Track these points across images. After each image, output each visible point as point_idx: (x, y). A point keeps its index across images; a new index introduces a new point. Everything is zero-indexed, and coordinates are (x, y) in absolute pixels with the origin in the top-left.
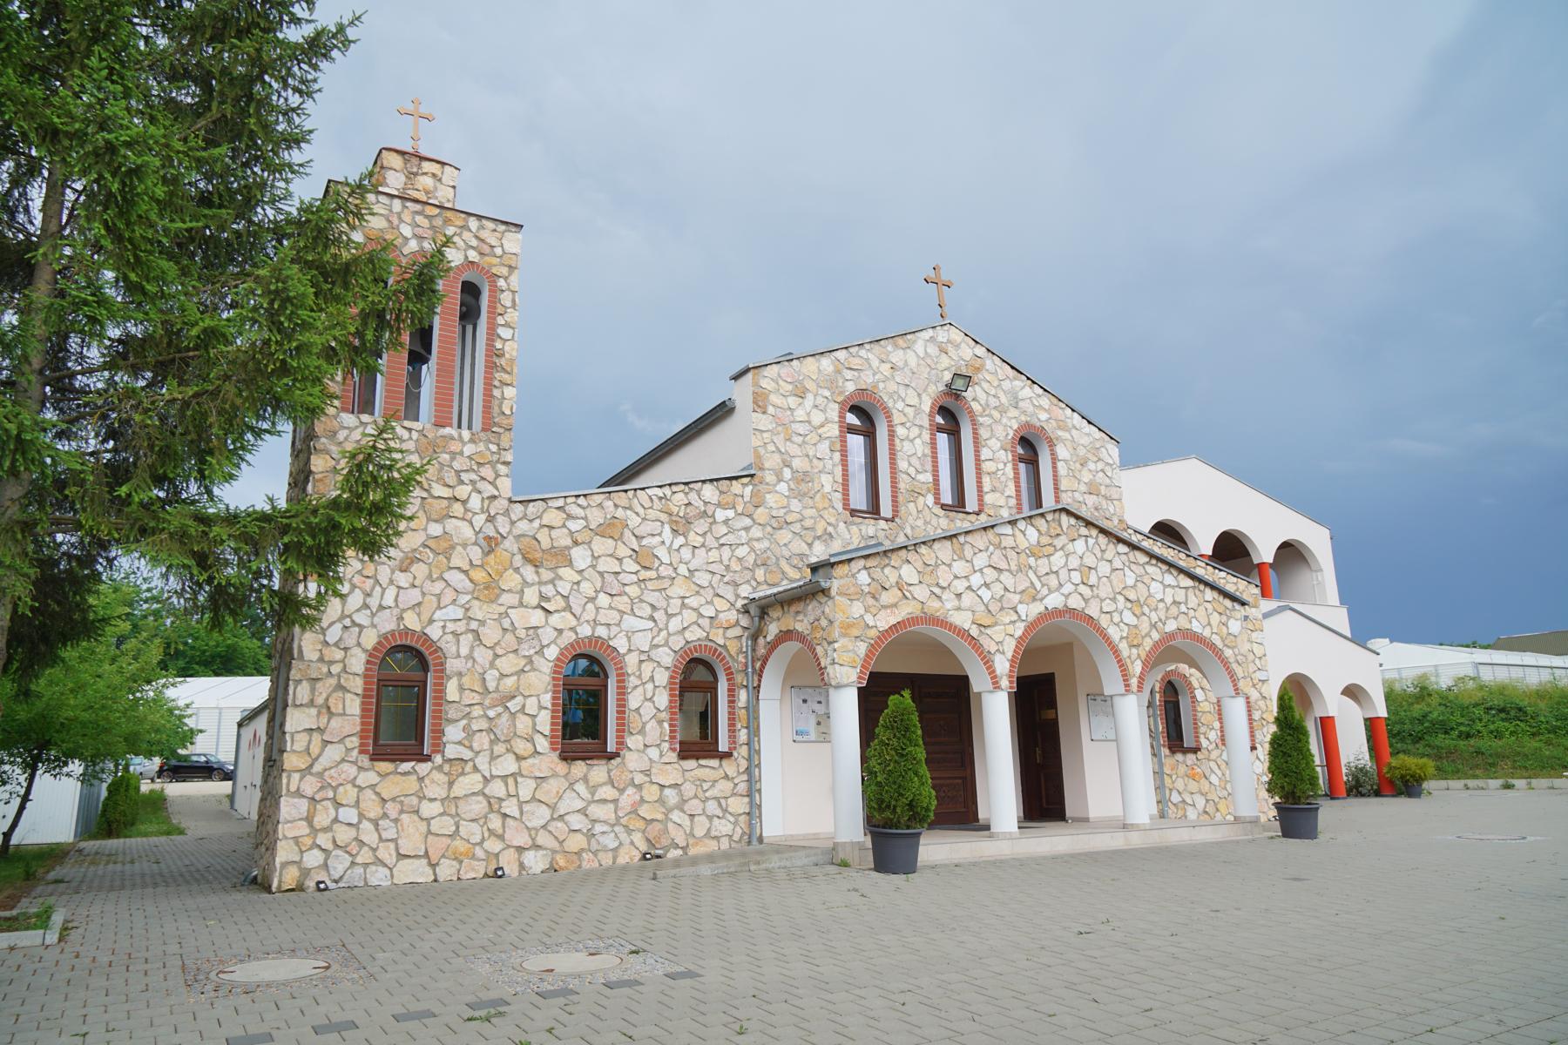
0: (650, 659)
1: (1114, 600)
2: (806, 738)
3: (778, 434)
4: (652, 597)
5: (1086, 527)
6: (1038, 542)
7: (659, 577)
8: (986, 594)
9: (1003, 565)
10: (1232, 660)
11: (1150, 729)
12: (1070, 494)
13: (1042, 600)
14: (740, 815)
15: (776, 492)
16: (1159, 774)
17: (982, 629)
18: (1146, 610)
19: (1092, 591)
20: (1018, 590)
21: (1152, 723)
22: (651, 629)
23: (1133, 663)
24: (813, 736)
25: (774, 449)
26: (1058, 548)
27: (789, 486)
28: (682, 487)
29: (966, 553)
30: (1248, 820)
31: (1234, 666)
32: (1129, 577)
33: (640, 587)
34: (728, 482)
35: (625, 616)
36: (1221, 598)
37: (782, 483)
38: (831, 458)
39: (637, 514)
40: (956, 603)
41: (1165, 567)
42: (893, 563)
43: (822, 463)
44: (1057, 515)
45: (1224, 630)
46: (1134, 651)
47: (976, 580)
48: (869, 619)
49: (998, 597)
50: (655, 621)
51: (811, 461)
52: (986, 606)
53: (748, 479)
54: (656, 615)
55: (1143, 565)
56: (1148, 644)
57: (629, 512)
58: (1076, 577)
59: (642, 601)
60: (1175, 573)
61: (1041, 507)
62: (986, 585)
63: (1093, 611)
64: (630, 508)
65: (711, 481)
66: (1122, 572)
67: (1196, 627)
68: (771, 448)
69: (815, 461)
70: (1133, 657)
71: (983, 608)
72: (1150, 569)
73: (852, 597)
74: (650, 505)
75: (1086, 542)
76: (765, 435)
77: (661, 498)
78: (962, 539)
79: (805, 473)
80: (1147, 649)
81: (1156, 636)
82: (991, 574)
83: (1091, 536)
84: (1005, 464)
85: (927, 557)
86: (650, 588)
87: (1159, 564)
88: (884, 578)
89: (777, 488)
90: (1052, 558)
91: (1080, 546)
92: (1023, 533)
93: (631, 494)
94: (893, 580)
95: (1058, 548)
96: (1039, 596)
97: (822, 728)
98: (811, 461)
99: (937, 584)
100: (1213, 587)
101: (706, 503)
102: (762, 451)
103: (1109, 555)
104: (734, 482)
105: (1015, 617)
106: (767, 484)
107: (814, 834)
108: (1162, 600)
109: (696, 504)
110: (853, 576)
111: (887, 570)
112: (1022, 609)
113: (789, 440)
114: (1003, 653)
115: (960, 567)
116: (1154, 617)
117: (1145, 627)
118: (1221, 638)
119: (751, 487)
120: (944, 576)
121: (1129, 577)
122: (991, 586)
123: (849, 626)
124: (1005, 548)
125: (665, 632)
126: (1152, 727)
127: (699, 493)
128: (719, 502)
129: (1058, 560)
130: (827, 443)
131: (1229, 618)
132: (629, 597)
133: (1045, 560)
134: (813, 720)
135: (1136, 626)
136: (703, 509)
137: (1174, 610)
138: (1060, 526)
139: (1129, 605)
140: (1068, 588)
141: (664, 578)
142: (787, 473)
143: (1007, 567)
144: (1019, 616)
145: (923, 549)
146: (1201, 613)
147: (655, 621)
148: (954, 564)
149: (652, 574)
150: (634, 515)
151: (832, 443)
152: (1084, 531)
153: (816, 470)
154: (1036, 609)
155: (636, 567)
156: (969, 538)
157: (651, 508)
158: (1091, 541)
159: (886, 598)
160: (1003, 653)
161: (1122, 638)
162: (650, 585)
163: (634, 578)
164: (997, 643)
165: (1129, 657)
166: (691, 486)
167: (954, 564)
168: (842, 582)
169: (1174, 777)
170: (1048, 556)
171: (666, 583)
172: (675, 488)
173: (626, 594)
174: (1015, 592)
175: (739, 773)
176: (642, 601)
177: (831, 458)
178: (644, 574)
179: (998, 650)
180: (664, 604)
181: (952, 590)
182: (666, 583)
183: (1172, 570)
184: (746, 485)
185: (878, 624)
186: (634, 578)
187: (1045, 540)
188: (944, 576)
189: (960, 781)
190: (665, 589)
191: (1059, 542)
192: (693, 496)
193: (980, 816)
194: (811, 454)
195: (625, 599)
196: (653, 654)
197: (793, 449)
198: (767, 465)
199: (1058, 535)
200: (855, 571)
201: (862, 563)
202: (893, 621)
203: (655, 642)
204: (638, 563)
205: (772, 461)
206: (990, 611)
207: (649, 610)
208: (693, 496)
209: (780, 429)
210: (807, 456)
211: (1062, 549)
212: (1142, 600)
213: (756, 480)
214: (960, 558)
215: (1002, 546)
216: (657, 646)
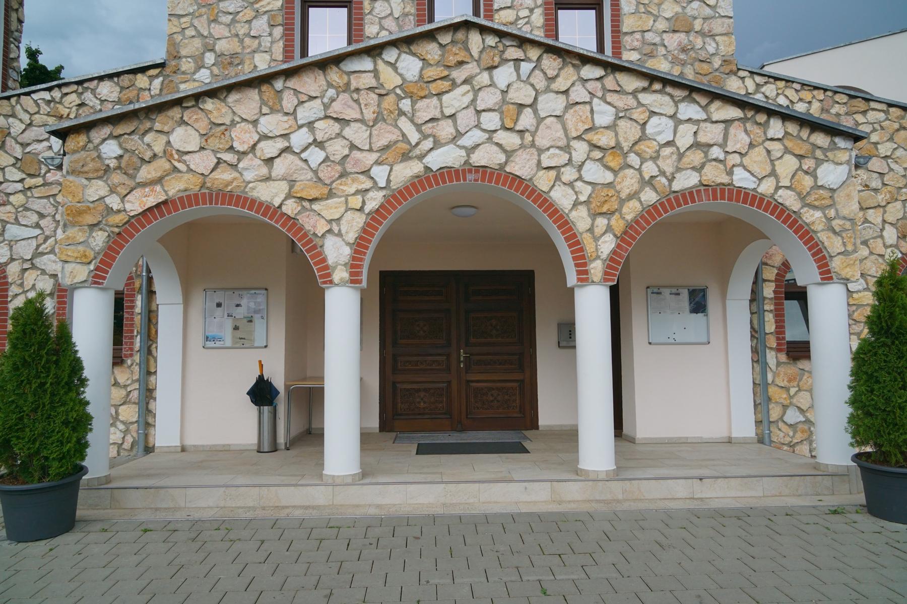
0: (34, 267)
1: (567, 149)
2: (218, 344)
3: (201, 16)
4: (37, 205)
5: (520, 46)
6: (421, 76)
7: (45, 184)
8: (315, 156)
9: (351, 113)
10: (818, 227)
11: (752, 327)
12: (638, 36)
13: (421, 157)
14: (132, 423)
15: (194, 80)
16: (761, 388)
17: (306, 204)
18: (633, 159)
19: (522, 138)
20: (375, 147)
21: (755, 322)
22: (36, 237)
23: (596, 239)
24: (228, 343)
25: (193, 33)
26: (459, 81)
27: (211, 72)
28: (75, 87)
29: (284, 103)
30: (831, 470)
31: (824, 237)
32: (602, 113)
33: (25, 195)
34: (131, 76)
35: (8, 226)
36: (805, 133)
37: (203, 70)
38: (270, 35)
39: (21, 120)
40: (264, 171)
41: (679, 93)
42: (158, 126)
43: (257, 41)
44: (460, 35)
45: (808, 181)
46: (601, 222)
47: (300, 138)
48: (114, 202)
49: (338, 158)
50: (42, 229)
51: (241, 41)
52: (315, 172)
53: (156, 71)
54: (43, 223)
55: (634, 93)
56: (631, 210)
57: (11, 120)
58: (491, 121)
59: (27, 209)
60: (703, 101)
61: (431, 19)
62: (320, 144)
63: (521, 167)
64: (13, 116)
65: (110, 76)
66: (588, 107)
67: (742, 179)
68: (190, 32)
69: (247, 41)
70: (598, 231)
71: (310, 175)
72: (646, 98)
73: (91, 175)
74: (36, 109)
75: (517, 69)
76: (183, 20)
77: (48, 102)
78: (279, 84)
79: (234, 55)
80: (629, 217)
81: (649, 196)
82: (325, 128)
83: (527, 59)
84: (531, 11)
85: (215, 113)
86: (36, 195)
87: (669, 89)
88: (142, 148)
89: (196, 76)
90: (445, 98)
91: (504, 75)
92: (393, 66)
93: (13, 100)
94: (158, 148)
95: (459, 81)
96: (417, 152)
97: (239, 334)
98: (241, 41)
99: (231, 148)
100: (786, 117)
101: (103, 102)
102: (178, 38)
103: (561, 84)
104: (139, 76)
105: (368, 184)
106: (184, 73)
107: (224, 446)
108: (669, 144)
109: (91, 104)
110: (96, 148)
111: (148, 138)
112: (380, 173)
113: (215, 21)
114: (339, 234)
115: (271, 123)
116: (650, 169)
117: (628, 182)
118: (799, 194)
119: (161, 79)
120: (243, 137)
121: (602, 113)
122: (326, 145)
123: (80, 213)
124: (357, 90)
125: (53, 239)
126: (756, 326)
127: (93, 91)
128: (119, 99)
129: (456, 99)
130: (265, 17)
131: (819, 162)
132: (14, 206)
133: (435, 100)
134: (229, 324)
135: (610, 185)
136: (99, 107)
137: (696, 157)
138: (467, 50)
139: (597, 154)
140: (476, 136)
141: (51, 184)
142: (210, 58)
143: (358, 116)
144: (375, 183)
145: (209, 104)
146: (757, 158)
147: (42, 229)
148: (263, 120)
149: (39, 181)
150: (18, 122)
151: (273, 17)
152: (514, 52)
153: (248, 50)
154: (406, 171)
155: (19, 175)
156: (293, 83)
157: (38, 113)
158: (526, 67)
159: (146, 173)
160: (339, 234)
161: (576, 204)
162: (36, 193)
163: (19, 186)
164: (330, 222)
165: (591, 230)
166: (85, 85)
167: (263, 120)
168: (76, 156)
169: (793, 391)
170: (439, 95)
171: (55, 190)
172: (65, 90)
173: (11, 203)
174: (371, 150)
175: (134, 381)
176: (27, 209)
177: (270, 35)
178: (30, 182)
179: (330, 231)
180: (51, 210)
181: (258, 153)
182: (55, 190)
183: (696, 96)
184: (157, 76)
185: (128, 206)
186: (19, 186)
187: (431, 73)
188: (243, 137)
189: (515, 385)
190: (54, 195)
191: (459, 75)
192: (88, 97)
193: (541, 423)
194: (241, 32)
195: (9, 208)
196: (37, 262)
197: (218, 30)
198: (183, 52)
199: (461, 63)
200: (96, 141)
201: (106, 130)
202: (151, 201)
203: (40, 249)
204: (23, 171)
205: (191, 47)
206: (320, 179)
207: (35, 218)
208: (88, 96)
209: (204, 10)
210: (237, 35)
211: (465, 82)
212: (626, 146)
213: (167, 71)
214: (273, 111)
215: (352, 88)
216: (43, 254)
